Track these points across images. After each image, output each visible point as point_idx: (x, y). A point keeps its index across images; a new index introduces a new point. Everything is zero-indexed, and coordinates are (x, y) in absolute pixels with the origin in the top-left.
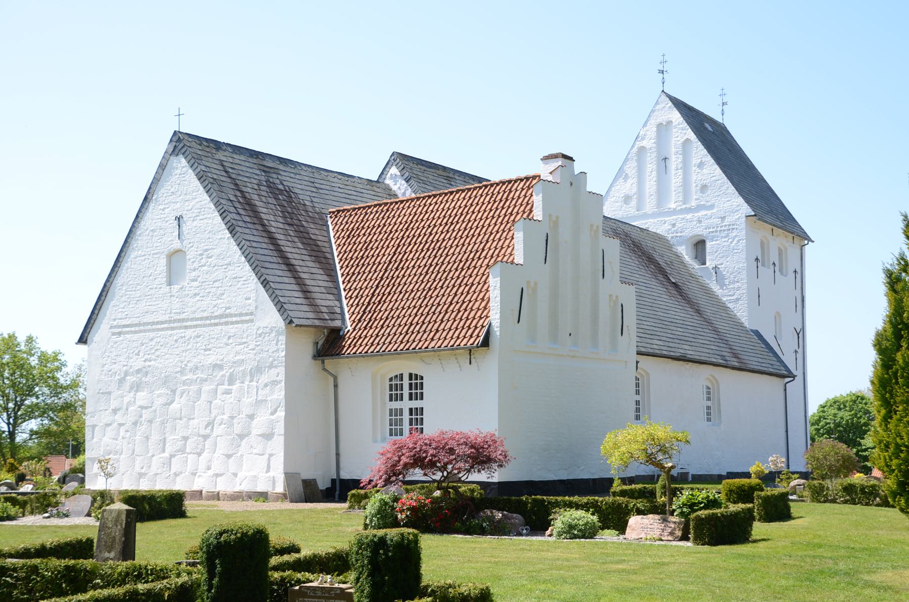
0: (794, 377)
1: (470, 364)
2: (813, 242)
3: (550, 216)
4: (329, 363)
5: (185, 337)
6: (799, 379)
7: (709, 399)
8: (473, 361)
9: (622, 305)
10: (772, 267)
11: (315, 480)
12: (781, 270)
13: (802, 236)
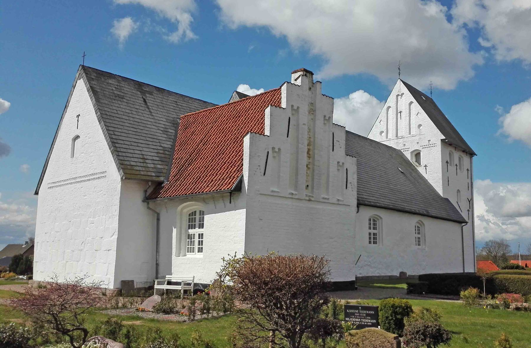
0: (467, 223)
1: (230, 203)
2: (476, 155)
3: (292, 106)
4: (151, 204)
5: (76, 188)
6: (470, 224)
7: (419, 233)
8: (232, 200)
9: (347, 169)
10: (456, 167)
11: (132, 281)
12: (460, 169)
13: (471, 154)
